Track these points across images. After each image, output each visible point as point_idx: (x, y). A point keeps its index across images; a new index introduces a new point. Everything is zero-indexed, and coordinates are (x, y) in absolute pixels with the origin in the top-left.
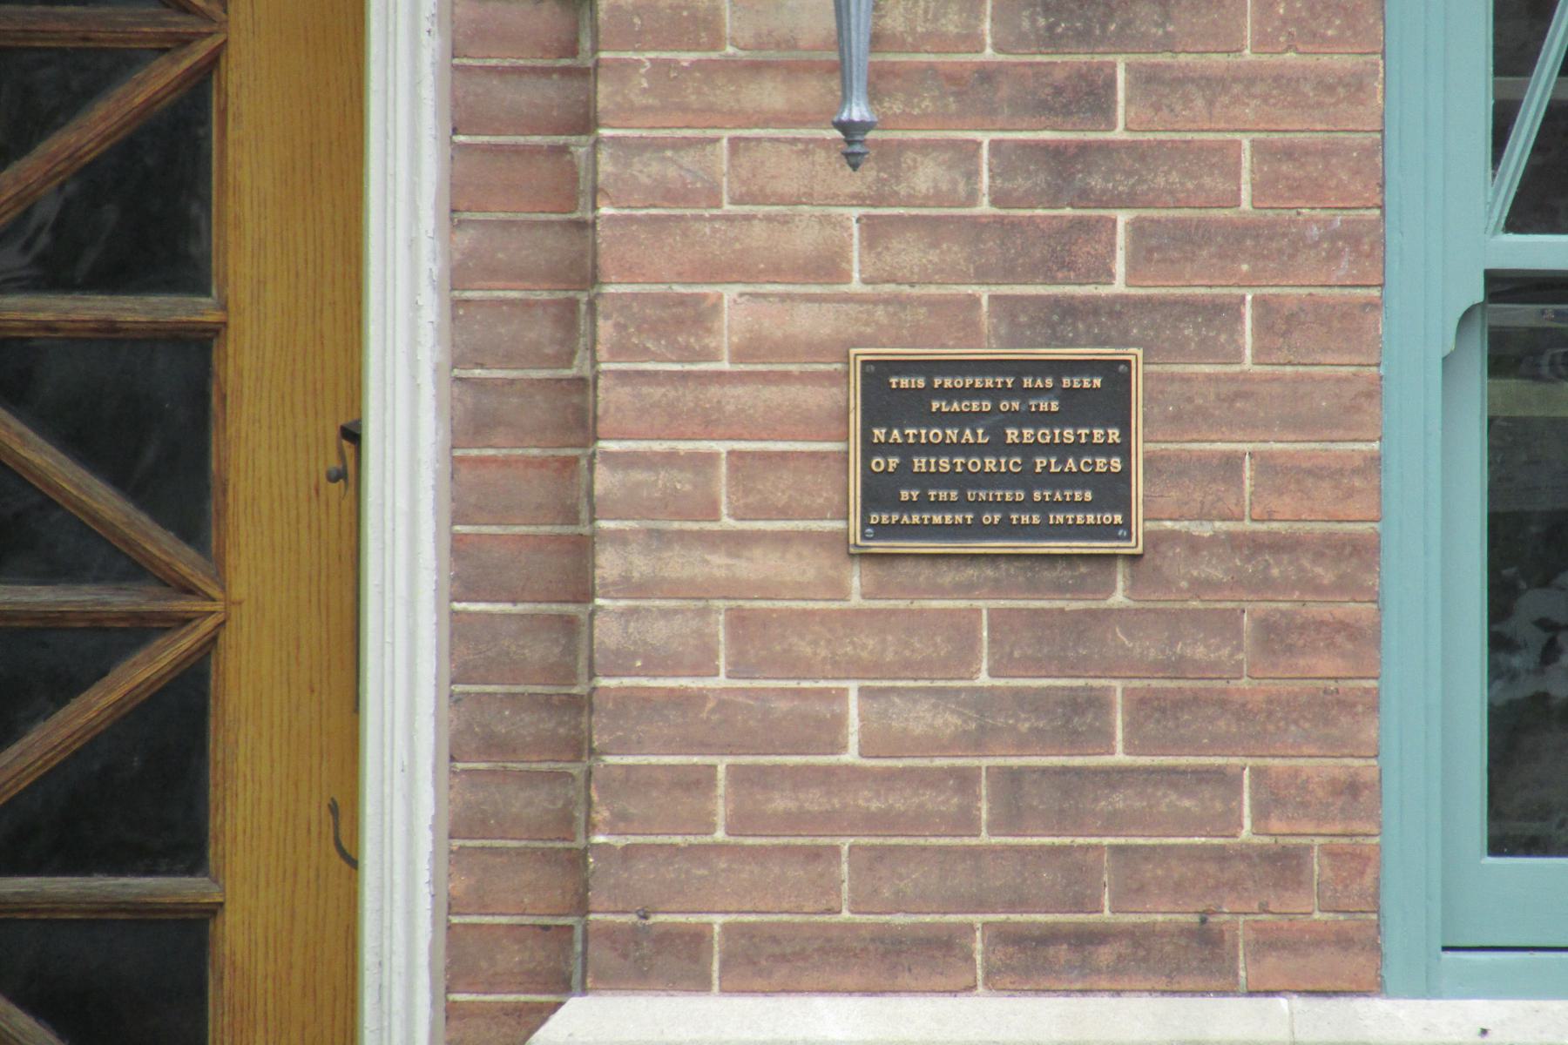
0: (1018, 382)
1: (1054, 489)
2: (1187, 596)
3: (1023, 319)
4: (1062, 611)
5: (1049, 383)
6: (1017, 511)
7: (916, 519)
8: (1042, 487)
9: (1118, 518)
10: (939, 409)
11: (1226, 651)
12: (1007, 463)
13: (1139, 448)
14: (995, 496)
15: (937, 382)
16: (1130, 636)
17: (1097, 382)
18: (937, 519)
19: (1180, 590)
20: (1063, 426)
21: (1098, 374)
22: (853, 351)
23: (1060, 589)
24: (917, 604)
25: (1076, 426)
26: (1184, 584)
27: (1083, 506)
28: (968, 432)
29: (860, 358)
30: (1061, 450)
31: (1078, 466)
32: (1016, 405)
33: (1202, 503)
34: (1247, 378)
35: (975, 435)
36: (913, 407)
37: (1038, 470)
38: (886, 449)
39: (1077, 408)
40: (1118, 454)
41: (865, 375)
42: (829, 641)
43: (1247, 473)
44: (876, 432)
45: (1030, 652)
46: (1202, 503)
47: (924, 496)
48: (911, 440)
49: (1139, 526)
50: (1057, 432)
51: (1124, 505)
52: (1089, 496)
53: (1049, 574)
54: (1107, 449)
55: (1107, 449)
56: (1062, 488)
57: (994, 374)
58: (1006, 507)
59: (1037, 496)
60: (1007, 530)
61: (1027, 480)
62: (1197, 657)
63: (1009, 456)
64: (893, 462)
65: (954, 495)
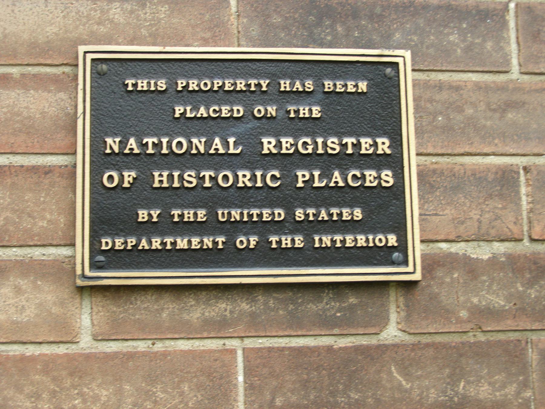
0: (274, 84)
1: (317, 206)
2: (468, 327)
3: (276, 19)
4: (329, 349)
5: (309, 85)
6: (276, 233)
7: (156, 244)
8: (304, 205)
9: (392, 240)
10: (183, 114)
11: (511, 389)
12: (264, 177)
13: (412, 163)
14: (250, 216)
15: (181, 84)
16: (407, 375)
17: (363, 86)
18: (182, 244)
19: (460, 321)
20: (326, 134)
21: (364, 78)
22: (82, 49)
23: (327, 323)
24: (159, 346)
25: (340, 135)
26: (464, 314)
27: (351, 226)
28: (217, 140)
29: (89, 57)
30: (327, 162)
31: (345, 180)
32: (272, 110)
33: (479, 221)
34: (518, 89)
35: (226, 144)
36: (154, 111)
37: (300, 184)
38: (121, 160)
39: (343, 113)
40: (389, 167)
41: (97, 75)
42: (54, 393)
43: (523, 190)
44: (109, 141)
45: (294, 398)
46: (479, 221)
47: (165, 216)
48: (335, 218)
49: (417, 249)
50: (320, 140)
51: (399, 227)
52: (358, 214)
53: (313, 307)
54: (377, 161)
55: (377, 161)
56: (328, 205)
57: (245, 75)
58: (262, 227)
59: (299, 214)
60: (265, 256)
61: (287, 195)
62: (481, 397)
63: (266, 169)
64: (129, 176)
65: (202, 214)
